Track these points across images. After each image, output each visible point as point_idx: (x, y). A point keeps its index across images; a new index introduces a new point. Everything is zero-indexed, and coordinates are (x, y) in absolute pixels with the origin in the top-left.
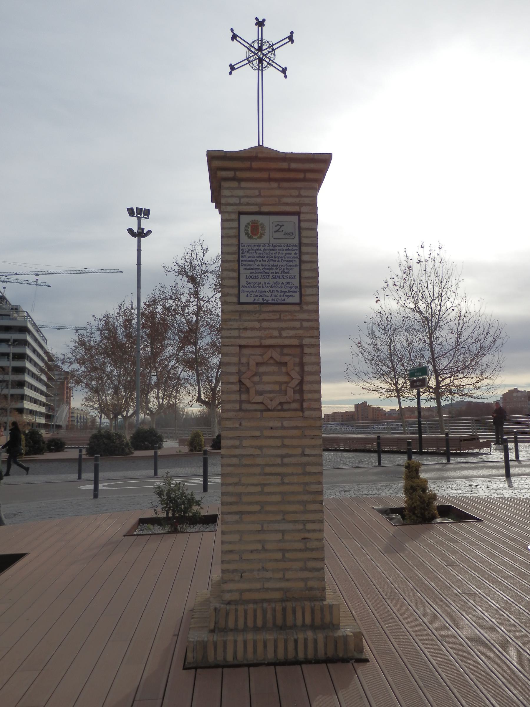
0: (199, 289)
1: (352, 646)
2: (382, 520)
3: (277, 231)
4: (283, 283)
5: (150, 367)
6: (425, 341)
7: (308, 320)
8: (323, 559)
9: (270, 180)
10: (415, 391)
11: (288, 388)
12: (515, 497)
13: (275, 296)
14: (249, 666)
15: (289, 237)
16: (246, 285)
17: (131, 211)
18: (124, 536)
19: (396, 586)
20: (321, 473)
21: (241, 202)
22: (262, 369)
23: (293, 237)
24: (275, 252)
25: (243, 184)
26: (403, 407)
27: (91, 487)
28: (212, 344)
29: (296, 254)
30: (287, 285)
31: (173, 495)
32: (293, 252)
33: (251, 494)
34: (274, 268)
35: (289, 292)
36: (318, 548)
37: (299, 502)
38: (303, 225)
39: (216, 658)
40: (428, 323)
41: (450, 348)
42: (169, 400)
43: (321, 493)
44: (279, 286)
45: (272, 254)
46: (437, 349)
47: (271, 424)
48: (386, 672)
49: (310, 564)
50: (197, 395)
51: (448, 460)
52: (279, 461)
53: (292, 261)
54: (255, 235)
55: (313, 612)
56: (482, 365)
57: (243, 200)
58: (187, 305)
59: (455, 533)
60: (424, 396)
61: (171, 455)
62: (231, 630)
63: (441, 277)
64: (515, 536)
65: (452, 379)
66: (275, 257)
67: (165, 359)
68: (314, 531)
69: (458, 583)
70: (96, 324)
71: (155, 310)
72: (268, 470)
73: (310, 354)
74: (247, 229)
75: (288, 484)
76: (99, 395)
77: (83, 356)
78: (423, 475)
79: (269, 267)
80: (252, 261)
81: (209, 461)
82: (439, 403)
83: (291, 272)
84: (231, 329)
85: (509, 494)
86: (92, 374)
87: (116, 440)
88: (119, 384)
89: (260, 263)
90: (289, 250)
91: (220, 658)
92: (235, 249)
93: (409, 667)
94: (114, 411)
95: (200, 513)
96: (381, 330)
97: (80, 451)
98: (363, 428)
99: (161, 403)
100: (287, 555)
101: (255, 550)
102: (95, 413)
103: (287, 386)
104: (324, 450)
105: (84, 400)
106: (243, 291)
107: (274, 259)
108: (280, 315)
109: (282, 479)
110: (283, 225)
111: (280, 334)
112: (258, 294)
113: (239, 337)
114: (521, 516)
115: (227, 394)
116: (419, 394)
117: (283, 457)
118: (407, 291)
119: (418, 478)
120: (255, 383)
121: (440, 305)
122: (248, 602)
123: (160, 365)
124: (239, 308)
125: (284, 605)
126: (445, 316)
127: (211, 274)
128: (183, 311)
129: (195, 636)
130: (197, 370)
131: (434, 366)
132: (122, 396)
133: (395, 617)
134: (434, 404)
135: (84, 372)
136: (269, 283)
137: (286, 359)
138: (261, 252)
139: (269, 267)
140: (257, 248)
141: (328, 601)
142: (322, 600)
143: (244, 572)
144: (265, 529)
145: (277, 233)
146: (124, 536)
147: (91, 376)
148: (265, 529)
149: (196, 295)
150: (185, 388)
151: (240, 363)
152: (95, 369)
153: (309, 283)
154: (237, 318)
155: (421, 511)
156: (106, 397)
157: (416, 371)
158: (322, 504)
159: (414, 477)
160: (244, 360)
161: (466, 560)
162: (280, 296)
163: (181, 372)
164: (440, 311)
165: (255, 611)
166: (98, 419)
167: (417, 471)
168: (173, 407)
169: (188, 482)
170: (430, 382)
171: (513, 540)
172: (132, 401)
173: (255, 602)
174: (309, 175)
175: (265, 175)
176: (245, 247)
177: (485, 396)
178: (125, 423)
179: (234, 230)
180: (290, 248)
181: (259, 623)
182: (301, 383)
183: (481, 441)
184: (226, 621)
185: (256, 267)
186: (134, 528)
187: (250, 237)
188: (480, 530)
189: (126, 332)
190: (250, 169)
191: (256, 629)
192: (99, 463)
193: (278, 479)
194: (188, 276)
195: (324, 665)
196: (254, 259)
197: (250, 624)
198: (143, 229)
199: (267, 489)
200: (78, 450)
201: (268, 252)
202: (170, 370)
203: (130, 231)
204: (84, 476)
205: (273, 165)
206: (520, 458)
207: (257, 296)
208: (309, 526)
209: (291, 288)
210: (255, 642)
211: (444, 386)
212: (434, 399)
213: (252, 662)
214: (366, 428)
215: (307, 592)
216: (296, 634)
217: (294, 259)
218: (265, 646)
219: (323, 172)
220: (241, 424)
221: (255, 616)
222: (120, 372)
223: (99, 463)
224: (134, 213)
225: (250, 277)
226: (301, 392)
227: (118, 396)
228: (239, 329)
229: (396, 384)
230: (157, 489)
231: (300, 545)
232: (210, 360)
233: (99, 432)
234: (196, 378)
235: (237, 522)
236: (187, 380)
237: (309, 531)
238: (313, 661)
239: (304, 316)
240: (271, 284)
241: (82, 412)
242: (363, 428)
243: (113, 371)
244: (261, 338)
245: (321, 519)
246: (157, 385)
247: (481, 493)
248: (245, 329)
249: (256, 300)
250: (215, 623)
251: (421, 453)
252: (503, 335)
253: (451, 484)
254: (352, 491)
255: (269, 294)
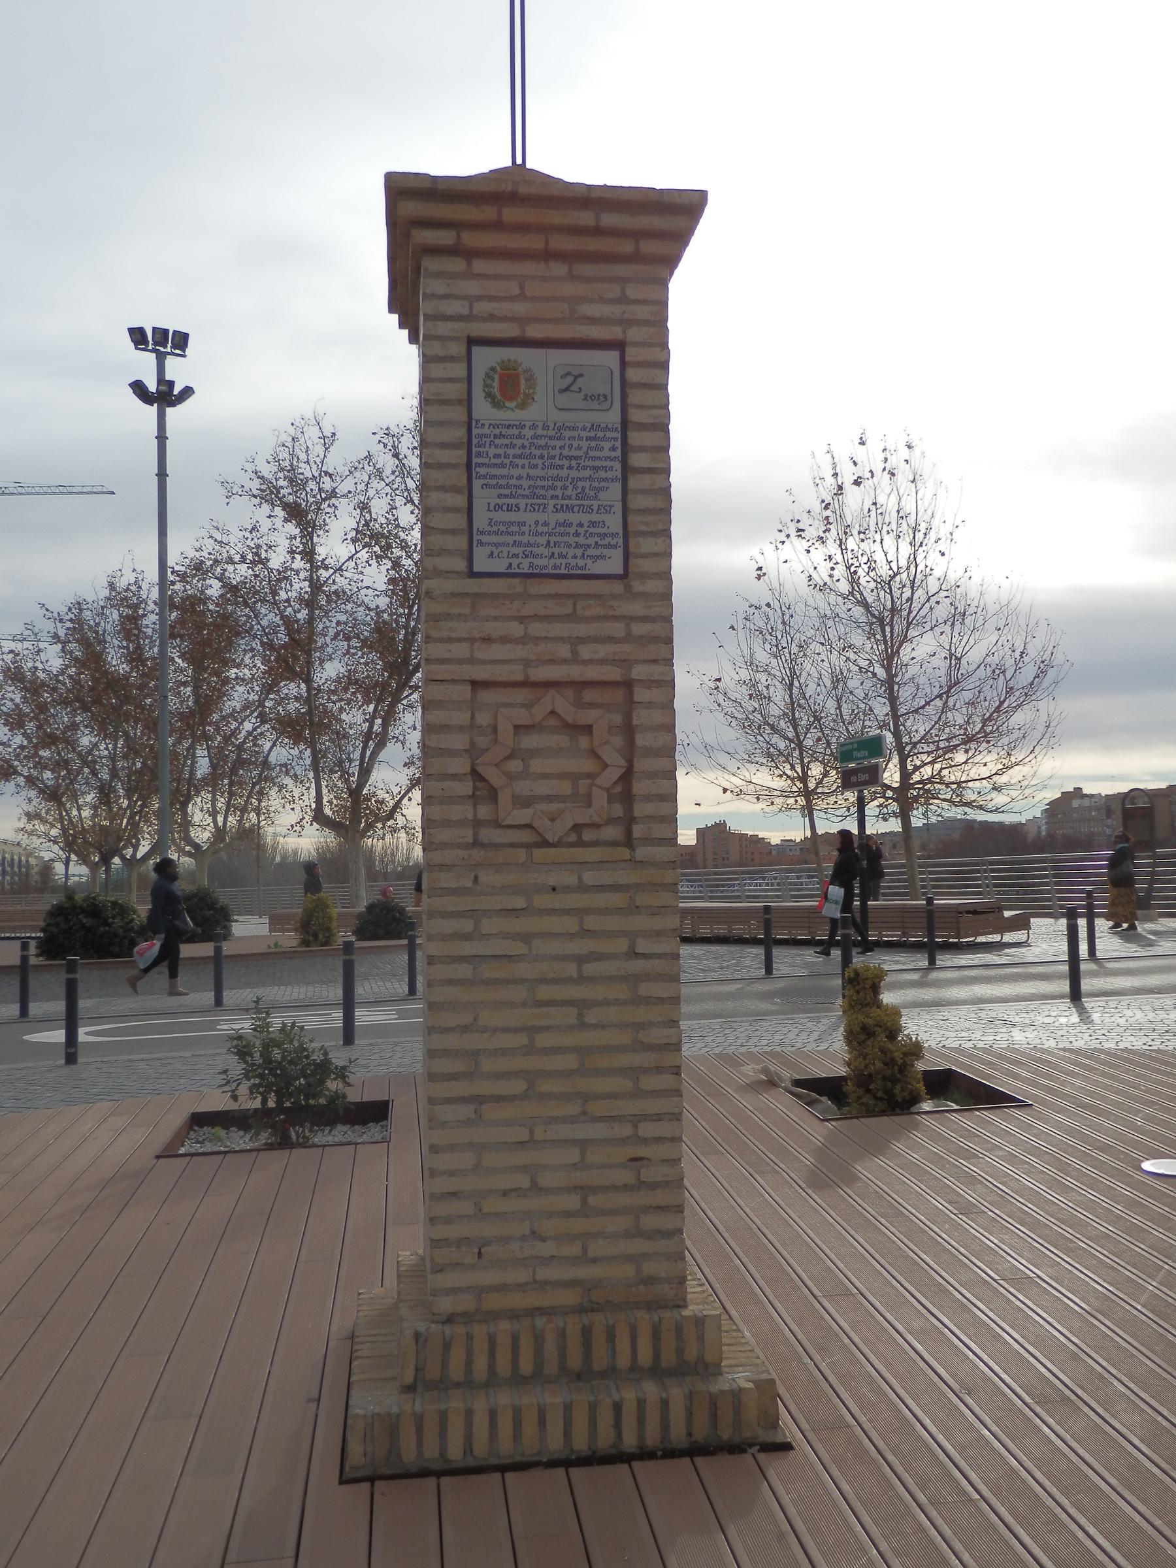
0: (315, 539)
1: (751, 1414)
2: (783, 1104)
3: (567, 389)
4: (581, 525)
5: (193, 735)
6: (875, 675)
7: (645, 619)
8: (679, 1209)
9: (548, 255)
10: (852, 796)
11: (595, 790)
12: (1099, 1046)
13: (561, 556)
14: (503, 1469)
15: (598, 407)
16: (489, 528)
17: (138, 336)
18: (158, 1157)
19: (841, 1266)
20: (676, 1000)
21: (475, 312)
22: (530, 741)
23: (605, 406)
24: (561, 443)
25: (479, 266)
26: (820, 832)
27: (58, 1036)
28: (349, 681)
29: (613, 449)
30: (592, 530)
31: (277, 1055)
32: (607, 445)
33: (504, 1052)
34: (559, 484)
35: (597, 545)
36: (667, 1183)
37: (622, 1071)
38: (633, 374)
39: (420, 1454)
40: (883, 631)
41: (936, 692)
42: (242, 817)
43: (677, 1047)
44: (572, 530)
45: (554, 448)
46: (904, 694)
47: (553, 879)
48: (836, 1472)
49: (650, 1222)
50: (314, 806)
51: (932, 961)
52: (571, 970)
53: (604, 468)
54: (511, 399)
55: (656, 1336)
56: (1009, 732)
57: (481, 308)
58: (286, 578)
59: (969, 1135)
60: (871, 809)
61: (255, 954)
62: (458, 1385)
63: (913, 516)
64: (1109, 1141)
65: (937, 766)
66: (562, 457)
67: (231, 715)
68: (659, 1140)
69: (984, 1252)
70: (49, 626)
71: (202, 592)
72: (545, 992)
73: (650, 705)
74: (489, 381)
75: (594, 1027)
76: (61, 805)
77: (17, 705)
78: (888, 998)
79: (545, 483)
80: (503, 466)
81: (359, 969)
82: (906, 822)
83: (601, 495)
84: (449, 640)
85: (1083, 1040)
86: (41, 753)
87: (114, 917)
88: (112, 780)
89: (523, 473)
90: (595, 438)
91: (431, 1451)
92: (459, 434)
93: (890, 1457)
94: (98, 845)
95: (344, 1096)
96: (768, 647)
97: (25, 946)
98: (718, 886)
99: (220, 824)
100: (592, 1200)
101: (515, 1190)
102: (50, 852)
103: (592, 784)
104: (686, 940)
105: (24, 819)
106: (481, 544)
107: (557, 462)
108: (575, 605)
109: (580, 1016)
110: (581, 375)
111: (575, 653)
112: (519, 550)
113: (472, 661)
114: (1118, 1092)
115: (441, 804)
116: (861, 804)
117: (581, 960)
118: (832, 552)
119: (878, 1004)
120: (510, 777)
121: (912, 587)
122: (495, 1315)
123: (218, 729)
124: (472, 585)
125: (585, 1321)
126: (922, 613)
127: (344, 501)
128: (274, 593)
129: (371, 1402)
130: (312, 744)
131: (897, 735)
132: (120, 808)
133: (846, 1341)
134: (895, 825)
135: (22, 747)
136: (546, 524)
137: (589, 716)
138: (526, 443)
139: (545, 483)
140: (515, 432)
141: (692, 1310)
142: (679, 1306)
143: (487, 1243)
144: (537, 1137)
145: (567, 393)
146: (158, 1157)
147: (41, 758)
148: (537, 1137)
149: (309, 554)
150: (282, 787)
151: (473, 726)
152: (50, 740)
153: (646, 524)
154: (467, 611)
155: (885, 1084)
156: (79, 810)
157: (856, 746)
158: (678, 1074)
159: (867, 1005)
160: (483, 719)
161: (1002, 1201)
162: (575, 557)
163: (271, 748)
164: (910, 599)
165: (515, 1339)
166: (59, 868)
167: (876, 990)
168: (250, 836)
169: (309, 1021)
170: (886, 775)
171: (1105, 1148)
172: (146, 821)
173: (514, 1315)
174: (647, 247)
175: (535, 242)
176: (486, 431)
177: (1017, 806)
178: (130, 877)
179: (457, 385)
180: (601, 434)
181: (526, 1366)
182: (627, 777)
183: (1007, 914)
184: (445, 1365)
185: (514, 482)
186: (180, 1137)
187: (496, 404)
188: (1028, 1128)
189: (127, 648)
190: (497, 226)
191: (518, 1380)
192: (78, 976)
193: (569, 1016)
194: (286, 506)
195: (686, 1461)
196: (507, 461)
197: (503, 1367)
198: (171, 384)
199: (543, 1041)
200: (18, 944)
201: (542, 442)
202: (244, 742)
203: (138, 388)
204: (35, 1008)
205: (555, 217)
206: (1098, 954)
207: (516, 556)
208: (648, 1130)
209: (603, 536)
210: (517, 1412)
211: (918, 782)
212: (895, 814)
213: (509, 1461)
214: (723, 886)
215: (641, 1287)
216: (617, 1390)
217: (608, 463)
218: (542, 1422)
219: (682, 238)
220: (476, 878)
221: (515, 1348)
222: (115, 749)
223: (78, 976)
224: (146, 342)
225: (497, 508)
226: (627, 798)
227: (110, 809)
228: (472, 640)
229: (804, 778)
230: (235, 1043)
231: (625, 1176)
232: (344, 716)
233: (70, 898)
234: (308, 761)
235: (468, 1123)
236: (286, 768)
237: (645, 1141)
238: (660, 1453)
239: (636, 608)
240: (552, 525)
241: (17, 850)
242: (718, 886)
243: (96, 745)
244: (527, 663)
245: (677, 1111)
246: (212, 781)
247: (1001, 1039)
248: (487, 640)
249: (514, 565)
250: (417, 1370)
251: (868, 947)
252: (1059, 658)
253: (952, 1017)
254: (709, 1039)
255: (546, 552)
